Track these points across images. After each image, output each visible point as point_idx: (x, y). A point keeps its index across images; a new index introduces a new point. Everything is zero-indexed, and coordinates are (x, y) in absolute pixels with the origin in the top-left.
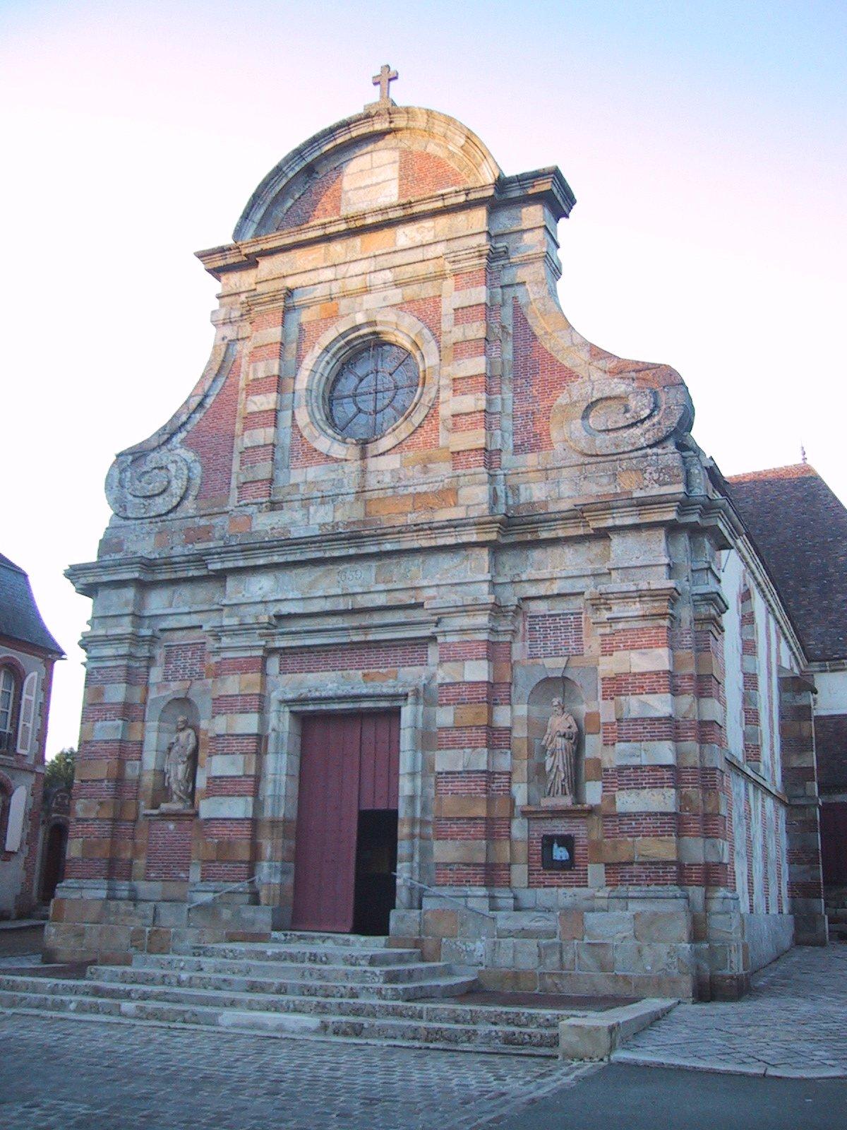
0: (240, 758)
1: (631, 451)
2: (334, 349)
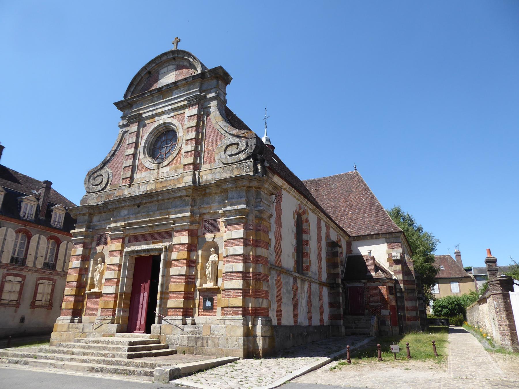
0: (113, 272)
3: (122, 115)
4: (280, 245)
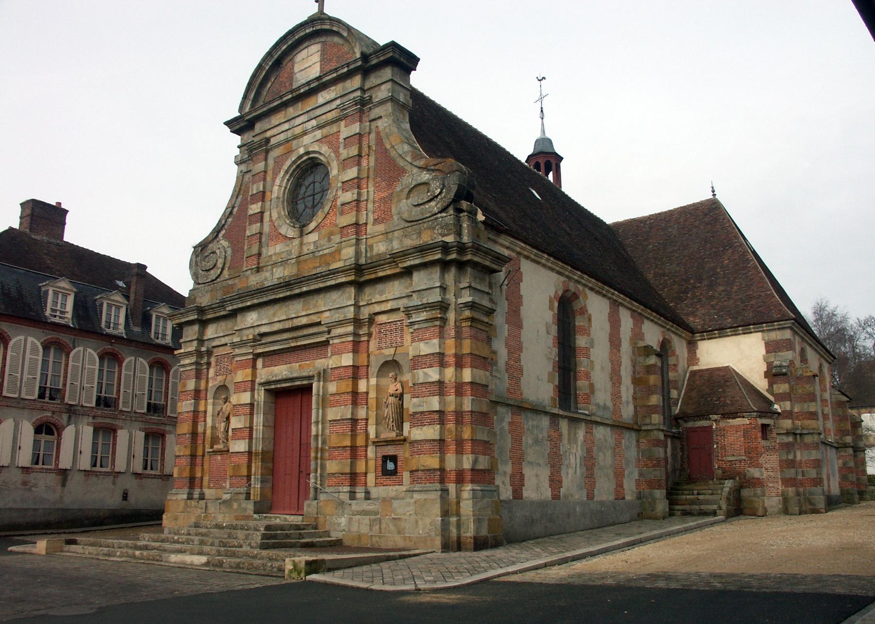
0: (243, 418)
1: (430, 217)
2: (291, 171)
3: (239, 143)
4: (518, 360)
